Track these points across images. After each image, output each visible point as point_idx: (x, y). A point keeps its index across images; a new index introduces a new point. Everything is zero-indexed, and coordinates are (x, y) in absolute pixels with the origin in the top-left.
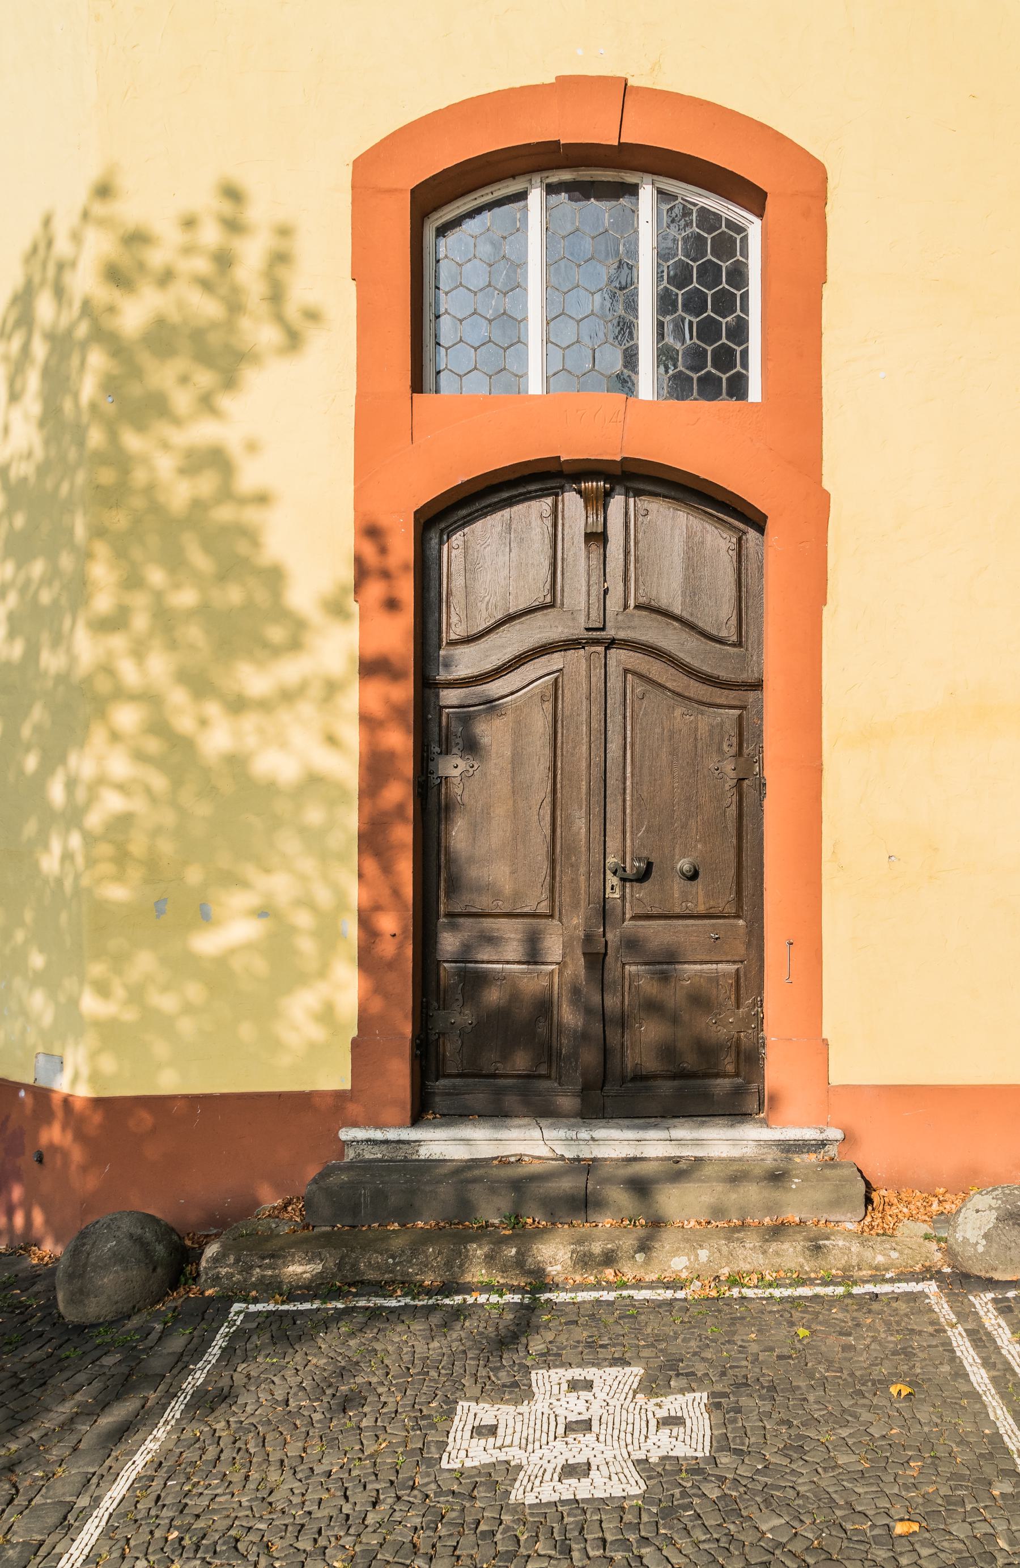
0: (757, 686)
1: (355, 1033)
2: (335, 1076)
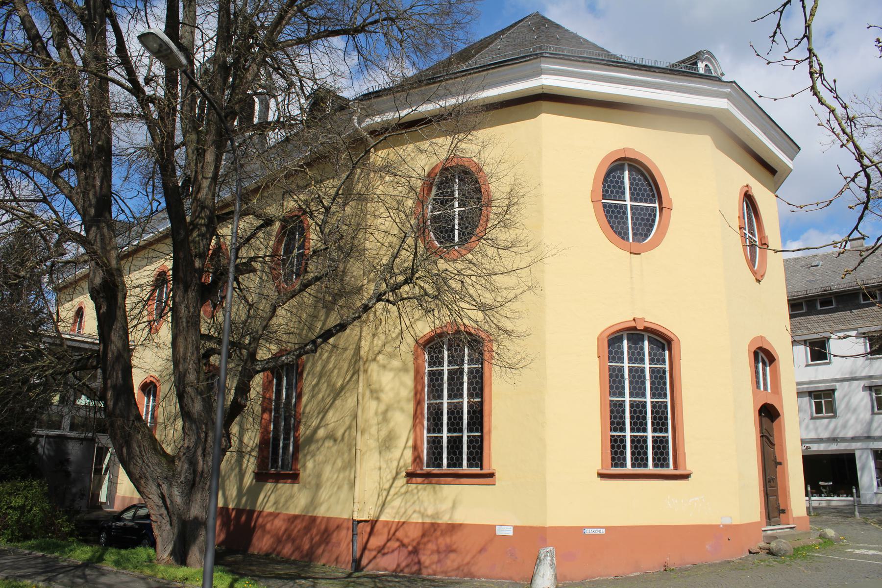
2: (759, 520)
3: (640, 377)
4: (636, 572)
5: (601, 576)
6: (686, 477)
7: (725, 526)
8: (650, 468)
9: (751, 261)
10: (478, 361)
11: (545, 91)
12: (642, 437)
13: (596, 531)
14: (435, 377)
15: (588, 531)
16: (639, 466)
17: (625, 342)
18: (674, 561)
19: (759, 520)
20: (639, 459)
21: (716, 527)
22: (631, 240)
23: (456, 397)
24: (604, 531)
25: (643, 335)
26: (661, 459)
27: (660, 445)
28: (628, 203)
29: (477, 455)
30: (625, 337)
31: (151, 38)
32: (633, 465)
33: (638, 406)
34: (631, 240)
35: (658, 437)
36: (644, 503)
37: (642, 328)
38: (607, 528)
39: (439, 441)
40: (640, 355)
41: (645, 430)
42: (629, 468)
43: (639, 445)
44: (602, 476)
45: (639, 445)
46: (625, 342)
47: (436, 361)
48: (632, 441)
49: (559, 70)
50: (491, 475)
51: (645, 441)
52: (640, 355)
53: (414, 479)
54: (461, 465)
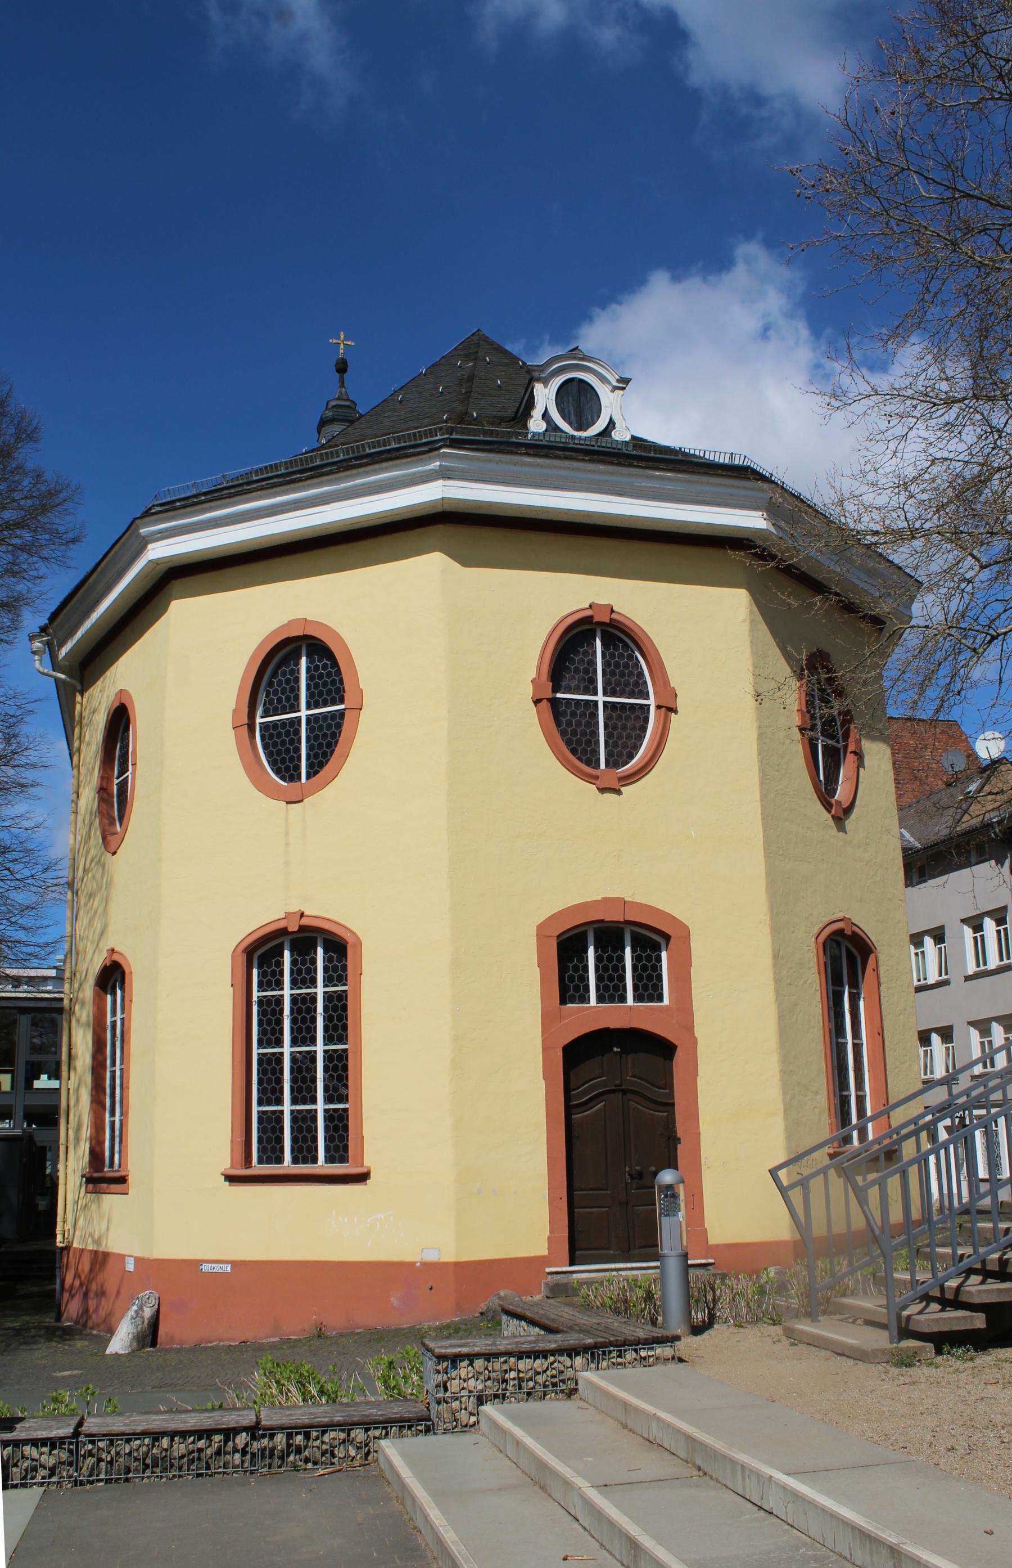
0: (673, 1104)
1: (548, 1233)
2: (541, 1249)
3: (273, 1012)
4: (273, 1337)
5: (220, 1341)
6: (362, 1178)
7: (424, 1264)
8: (321, 1165)
9: (825, 793)
12: (309, 1111)
13: (217, 1268)
15: (206, 1268)
17: (287, 954)
18: (335, 1321)
19: (541, 1249)
20: (304, 1152)
21: (412, 1264)
22: (603, 766)
23: (304, 1043)
24: (228, 1268)
25: (623, 929)
26: (338, 1151)
27: (339, 1126)
30: (287, 945)
31: (575, 384)
32: (295, 1160)
34: (603, 766)
35: (335, 1110)
36: (299, 1224)
37: (296, 929)
38: (234, 1264)
40: (298, 977)
41: (314, 1101)
42: (321, 1165)
44: (232, 1179)
46: (287, 954)
47: (272, 979)
49: (166, 530)
52: (298, 977)
53: (113, 1186)
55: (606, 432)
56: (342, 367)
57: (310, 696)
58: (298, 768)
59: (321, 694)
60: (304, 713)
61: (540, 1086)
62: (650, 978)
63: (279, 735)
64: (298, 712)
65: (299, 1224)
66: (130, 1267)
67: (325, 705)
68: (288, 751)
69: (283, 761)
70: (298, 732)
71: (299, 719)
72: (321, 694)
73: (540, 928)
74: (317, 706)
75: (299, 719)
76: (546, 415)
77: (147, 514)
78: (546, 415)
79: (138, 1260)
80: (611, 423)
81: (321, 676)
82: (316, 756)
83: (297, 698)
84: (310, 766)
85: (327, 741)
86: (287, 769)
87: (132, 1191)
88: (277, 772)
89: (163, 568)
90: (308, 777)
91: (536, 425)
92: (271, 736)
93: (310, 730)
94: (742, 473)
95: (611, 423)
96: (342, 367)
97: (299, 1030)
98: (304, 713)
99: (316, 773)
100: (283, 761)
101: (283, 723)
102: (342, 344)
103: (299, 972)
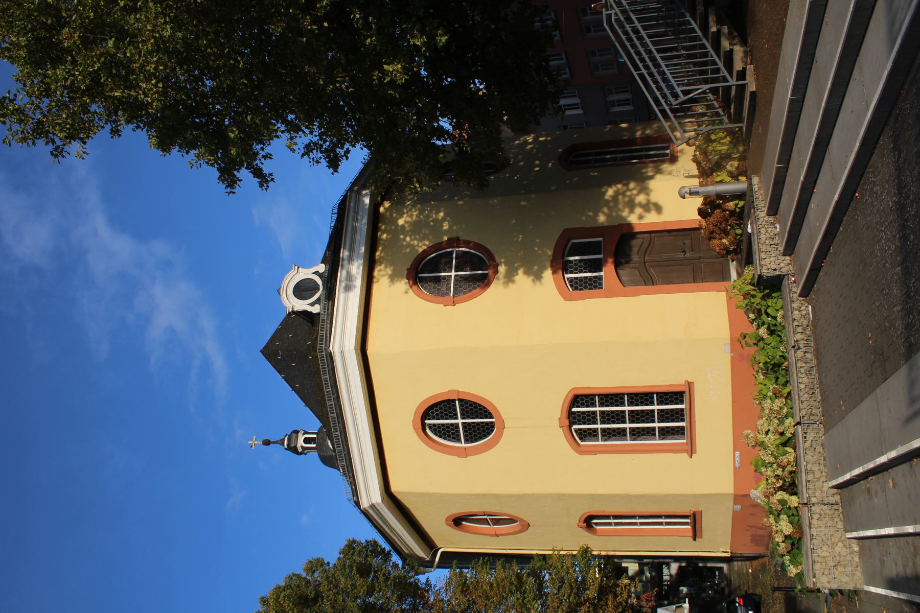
2: (723, 295)
10: (592, 399)
11: (359, 348)
13: (738, 459)
14: (596, 161)
15: (737, 465)
16: (683, 415)
19: (723, 295)
20: (678, 415)
21: (732, 358)
23: (624, 417)
24: (737, 453)
28: (453, 274)
29: (675, 396)
32: (683, 420)
33: (633, 417)
36: (713, 413)
38: (735, 450)
39: (662, 429)
41: (653, 411)
43: (665, 416)
45: (665, 416)
48: (662, 421)
50: (695, 539)
51: (662, 411)
54: (682, 410)
55: (320, 275)
56: (267, 443)
57: (451, 418)
58: (487, 423)
59: (450, 412)
60: (460, 421)
61: (643, 298)
62: (607, 401)
63: (471, 434)
64: (461, 420)
65: (713, 413)
66: (738, 507)
67: (456, 410)
68: (479, 429)
69: (483, 431)
70: (469, 424)
71: (463, 423)
72: (450, 412)
73: (566, 299)
74: (456, 414)
75: (463, 423)
76: (312, 304)
77: (357, 504)
78: (312, 304)
79: (735, 504)
80: (316, 273)
81: (441, 413)
82: (481, 414)
83: (452, 425)
84: (486, 417)
85: (474, 408)
86: (488, 429)
87: (700, 509)
88: (489, 434)
89: (385, 495)
90: (492, 418)
91: (316, 309)
92: (471, 438)
93: (468, 417)
94: (342, 207)
95: (316, 273)
96: (267, 443)
97: (618, 419)
98: (460, 421)
99: (490, 414)
100: (483, 431)
101: (465, 432)
102: (256, 442)
103: (589, 420)
